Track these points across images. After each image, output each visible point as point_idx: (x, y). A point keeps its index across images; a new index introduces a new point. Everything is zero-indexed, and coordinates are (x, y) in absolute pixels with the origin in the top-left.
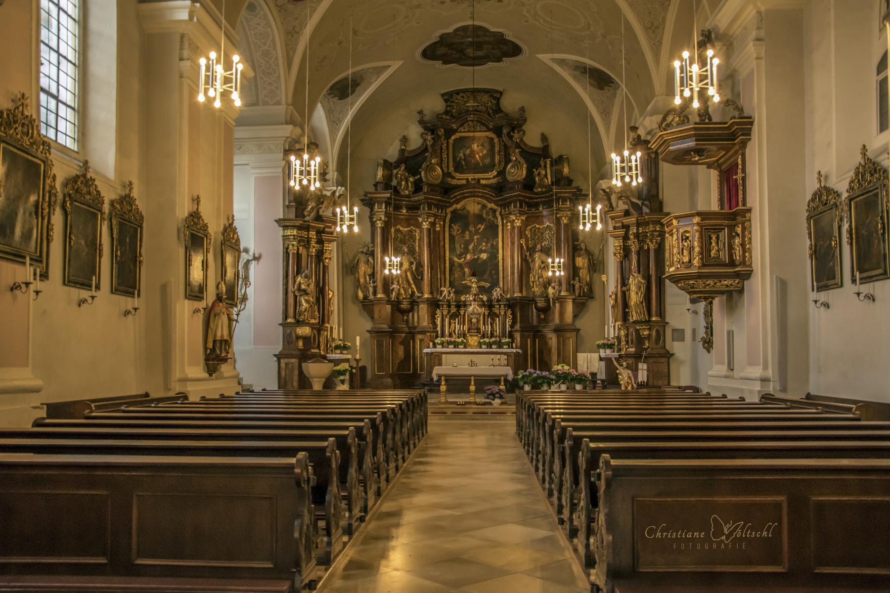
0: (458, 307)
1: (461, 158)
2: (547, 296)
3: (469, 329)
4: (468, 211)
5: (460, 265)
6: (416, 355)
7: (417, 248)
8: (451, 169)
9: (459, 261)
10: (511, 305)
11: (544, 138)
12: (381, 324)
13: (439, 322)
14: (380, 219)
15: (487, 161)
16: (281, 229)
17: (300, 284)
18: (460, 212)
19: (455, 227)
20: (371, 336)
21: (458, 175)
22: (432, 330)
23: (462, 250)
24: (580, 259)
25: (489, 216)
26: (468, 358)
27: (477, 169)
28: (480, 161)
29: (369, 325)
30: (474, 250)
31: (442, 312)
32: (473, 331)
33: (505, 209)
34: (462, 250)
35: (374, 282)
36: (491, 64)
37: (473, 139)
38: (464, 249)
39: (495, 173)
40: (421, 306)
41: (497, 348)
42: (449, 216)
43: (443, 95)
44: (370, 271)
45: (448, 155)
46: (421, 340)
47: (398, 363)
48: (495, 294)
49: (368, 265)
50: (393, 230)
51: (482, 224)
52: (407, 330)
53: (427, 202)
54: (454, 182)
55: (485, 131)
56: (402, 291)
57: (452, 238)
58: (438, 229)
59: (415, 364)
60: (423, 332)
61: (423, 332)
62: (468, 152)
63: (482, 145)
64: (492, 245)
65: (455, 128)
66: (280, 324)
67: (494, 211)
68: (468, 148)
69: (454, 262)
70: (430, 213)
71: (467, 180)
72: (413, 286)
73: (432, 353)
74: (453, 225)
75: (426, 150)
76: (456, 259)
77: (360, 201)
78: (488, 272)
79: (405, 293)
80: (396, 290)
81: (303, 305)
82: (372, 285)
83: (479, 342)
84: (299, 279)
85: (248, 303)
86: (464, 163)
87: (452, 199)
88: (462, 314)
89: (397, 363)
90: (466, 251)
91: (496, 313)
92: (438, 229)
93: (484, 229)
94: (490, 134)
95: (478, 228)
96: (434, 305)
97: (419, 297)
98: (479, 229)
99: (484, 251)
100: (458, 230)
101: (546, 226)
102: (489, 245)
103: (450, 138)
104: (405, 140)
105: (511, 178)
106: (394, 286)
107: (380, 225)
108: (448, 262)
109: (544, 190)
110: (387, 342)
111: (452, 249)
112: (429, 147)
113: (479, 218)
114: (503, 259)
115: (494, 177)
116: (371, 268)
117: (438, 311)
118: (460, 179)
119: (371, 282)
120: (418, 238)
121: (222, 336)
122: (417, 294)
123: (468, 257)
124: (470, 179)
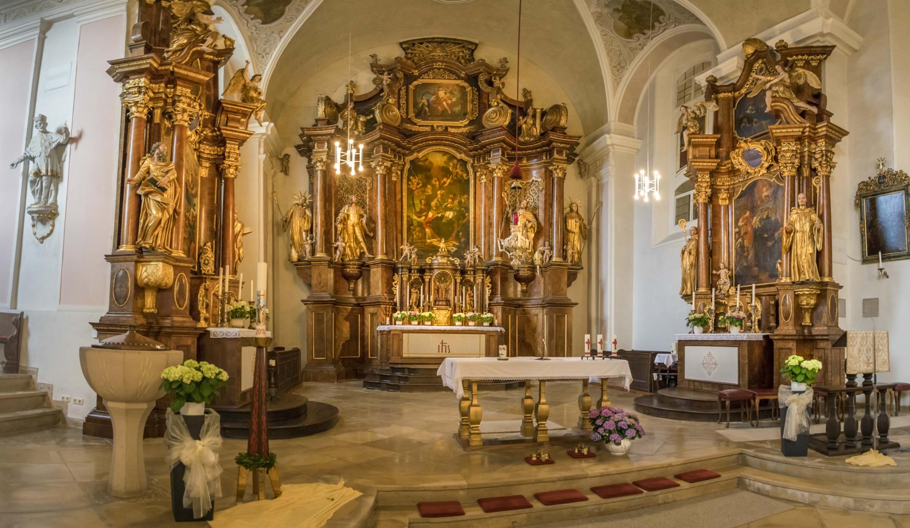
0: (422, 271)
1: (423, 104)
2: (533, 263)
3: (435, 301)
4: (431, 163)
5: (420, 224)
6: (366, 334)
7: (368, 200)
8: (412, 115)
9: (419, 219)
12: (321, 292)
13: (397, 290)
18: (421, 163)
19: (415, 180)
20: (308, 308)
21: (420, 121)
22: (388, 301)
23: (423, 207)
24: (573, 221)
25: (456, 169)
26: (436, 339)
27: (444, 116)
28: (448, 109)
29: (305, 295)
30: (437, 207)
31: (402, 278)
32: (440, 303)
33: (479, 161)
34: (423, 207)
35: (312, 239)
37: (440, 86)
38: (425, 205)
39: (466, 122)
40: (373, 270)
41: (462, 325)
42: (407, 166)
43: (401, 44)
44: (307, 226)
45: (407, 100)
46: (372, 315)
47: (343, 345)
48: (469, 257)
49: (305, 218)
51: (448, 178)
52: (353, 301)
53: (383, 144)
54: (415, 128)
56: (348, 251)
57: (411, 192)
58: (394, 179)
59: (364, 347)
60: (377, 304)
61: (377, 304)
62: (433, 98)
63: (451, 93)
64: (460, 202)
67: (464, 163)
68: (433, 95)
69: (412, 220)
70: (385, 156)
71: (432, 126)
72: (363, 244)
73: (389, 332)
74: (411, 178)
76: (415, 217)
77: (294, 148)
78: (454, 234)
79: (352, 254)
80: (341, 249)
82: (310, 242)
83: (451, 317)
85: (59, 221)
86: (427, 109)
87: (415, 144)
88: (427, 280)
89: (341, 344)
90: (428, 207)
91: (469, 281)
92: (394, 179)
93: (450, 184)
95: (442, 182)
96: (391, 269)
98: (445, 183)
99: (451, 209)
100: (418, 184)
101: (531, 181)
102: (456, 202)
103: (410, 83)
106: (339, 243)
107: (320, 168)
108: (405, 222)
109: (532, 139)
110: (328, 315)
111: (411, 205)
112: (385, 87)
113: (446, 172)
114: (475, 218)
115: (465, 126)
116: (308, 221)
117: (396, 277)
118: (421, 125)
119: (308, 238)
120: (368, 188)
122: (367, 255)
123: (430, 215)
124: (435, 126)
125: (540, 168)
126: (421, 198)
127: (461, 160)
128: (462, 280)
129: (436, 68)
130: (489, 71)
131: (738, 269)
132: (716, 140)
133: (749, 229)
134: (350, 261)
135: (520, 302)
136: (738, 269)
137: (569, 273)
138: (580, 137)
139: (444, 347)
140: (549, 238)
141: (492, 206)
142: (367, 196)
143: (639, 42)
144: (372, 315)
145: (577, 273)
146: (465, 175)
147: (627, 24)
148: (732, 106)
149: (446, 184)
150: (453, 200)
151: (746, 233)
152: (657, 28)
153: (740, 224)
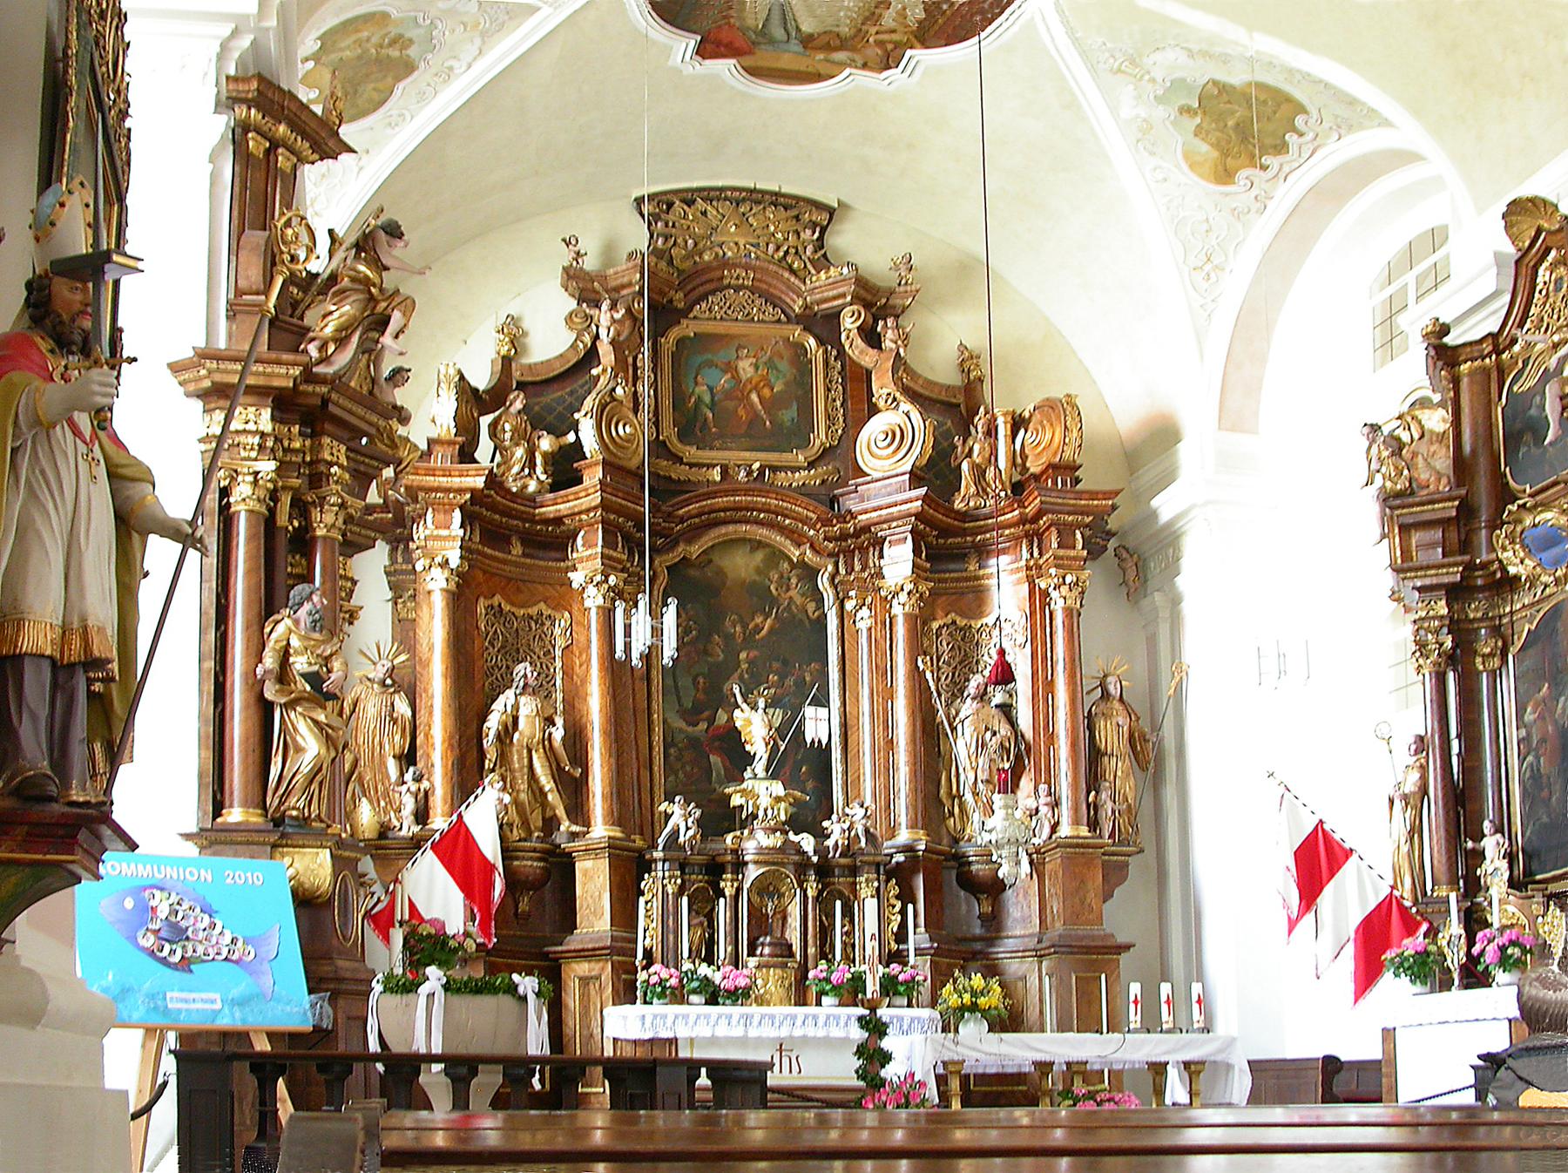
1: (699, 399)
4: (720, 572)
5: (694, 742)
8: (669, 432)
9: (690, 729)
10: (900, 875)
11: (967, 360)
14: (445, 564)
15: (789, 415)
16: (198, 405)
17: (285, 655)
18: (693, 572)
21: (691, 452)
23: (701, 695)
25: (788, 589)
34: (701, 695)
36: (853, 82)
43: (639, 201)
50: (481, 608)
55: (779, 321)
65: (681, 305)
66: (188, 836)
75: (592, 355)
81: (299, 750)
84: (281, 629)
94: (797, 332)
97: (574, 836)
98: (758, 629)
102: (790, 681)
104: (514, 334)
105: (872, 462)
108: (658, 738)
121: (74, 628)
125: (1019, 582)
126: (694, 671)
127: (802, 564)
128: (820, 892)
129: (729, 286)
130: (869, 297)
131: (1528, 834)
132: (1457, 503)
133: (1550, 728)
134: (520, 840)
135: (978, 946)
136: (1528, 834)
137: (1104, 863)
138: (1117, 493)
139: (785, 1061)
140: (1047, 776)
141: (890, 695)
142: (558, 664)
143: (1254, 192)
144: (586, 981)
145: (1127, 865)
146: (811, 607)
147: (1216, 145)
148: (1494, 395)
149: (764, 632)
150: (782, 678)
151: (1543, 741)
152: (1293, 148)
153: (1529, 716)
